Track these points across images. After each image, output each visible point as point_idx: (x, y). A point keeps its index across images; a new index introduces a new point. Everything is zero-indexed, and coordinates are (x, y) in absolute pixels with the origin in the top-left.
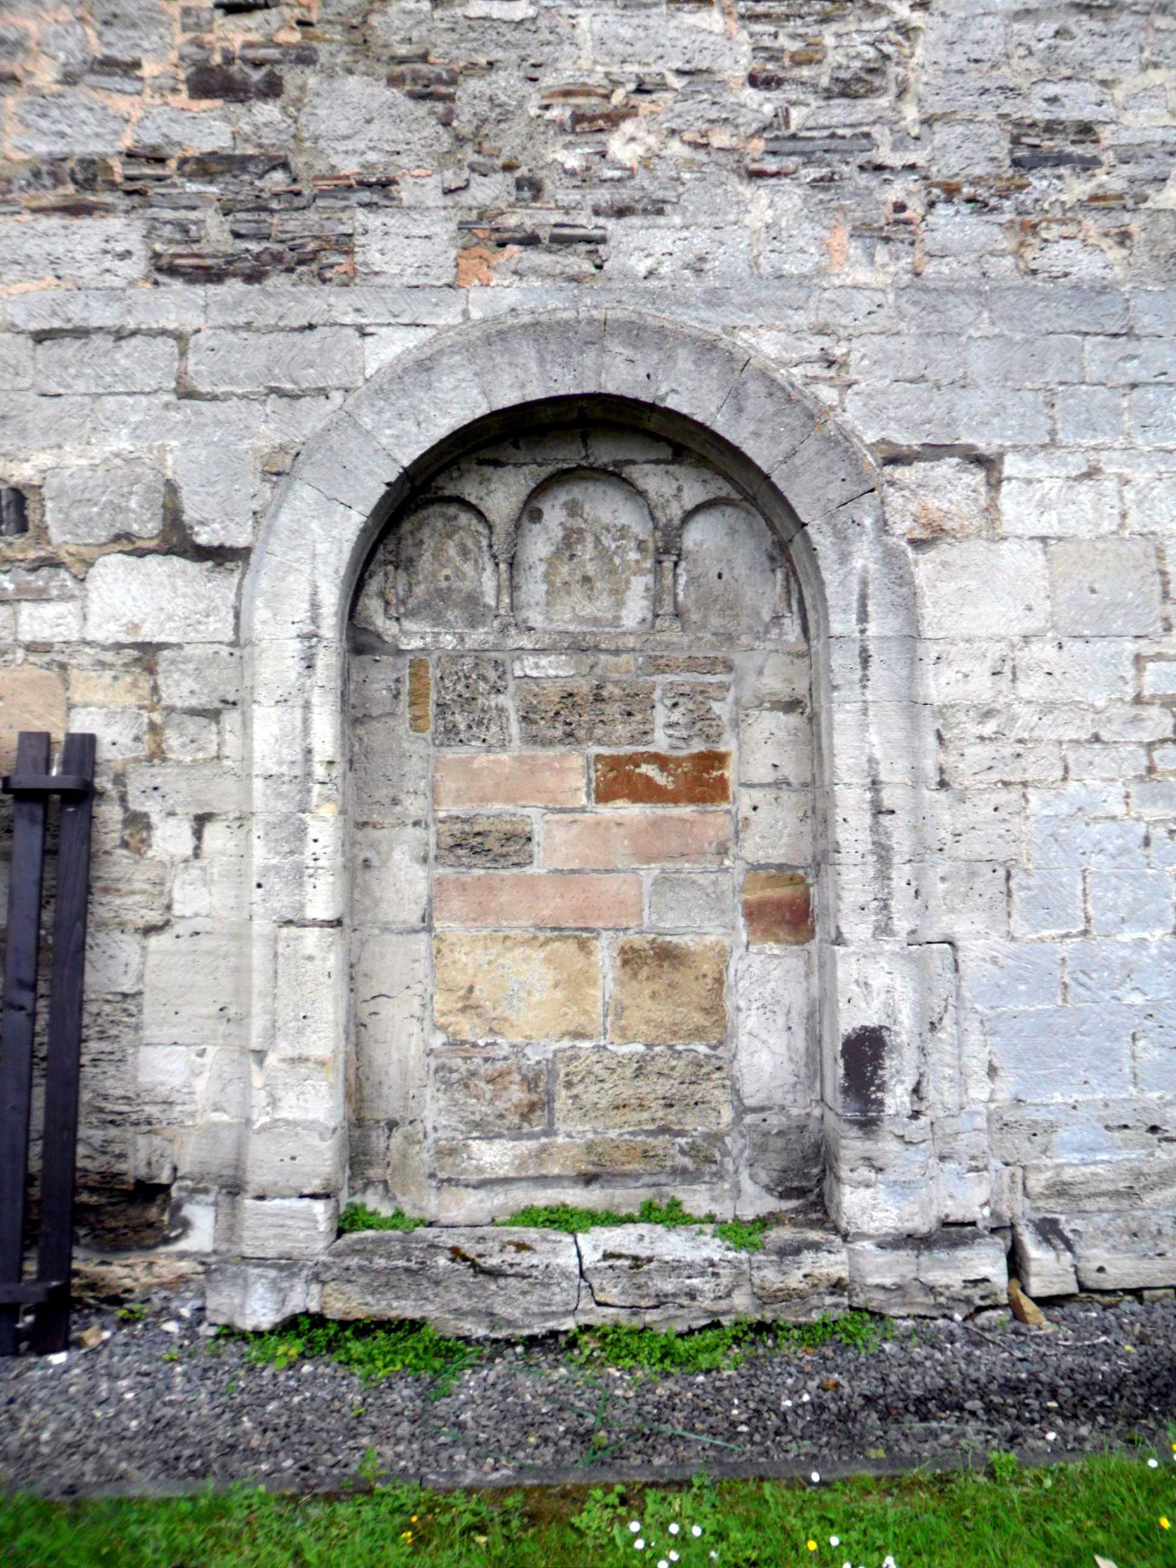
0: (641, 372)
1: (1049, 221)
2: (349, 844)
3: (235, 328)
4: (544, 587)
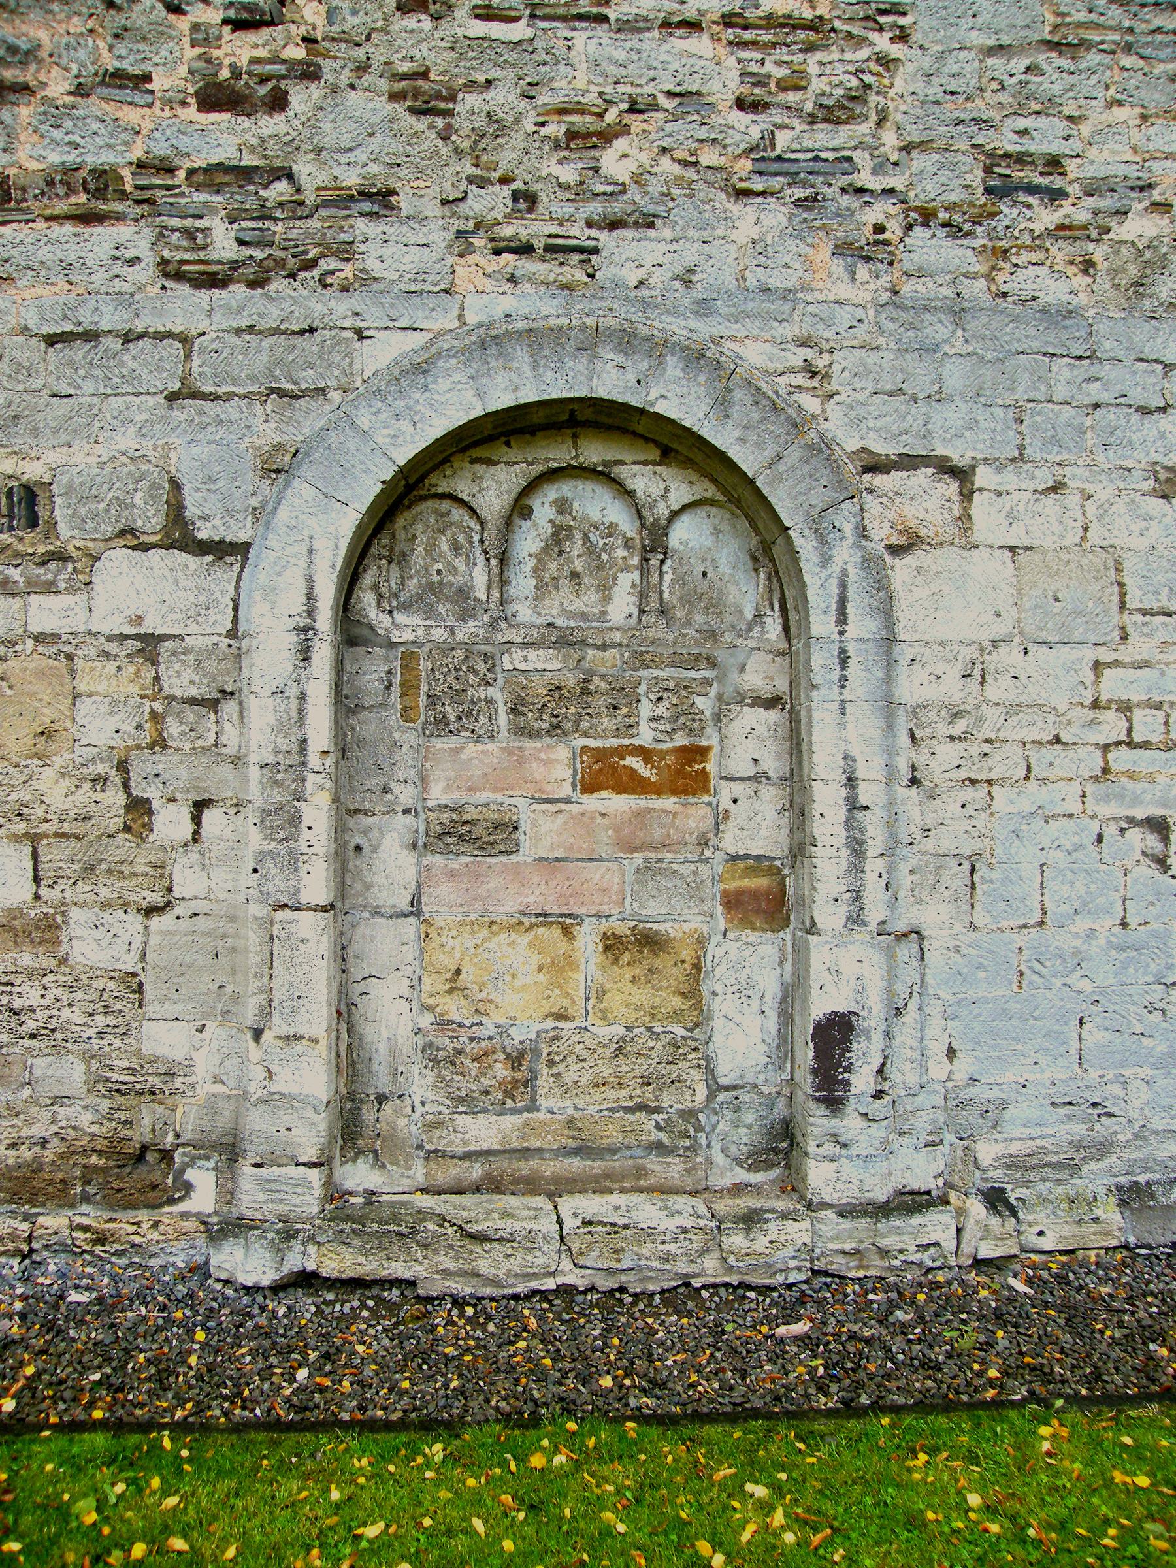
0: (631, 377)
1: (1019, 247)
2: (340, 830)
4: (534, 582)
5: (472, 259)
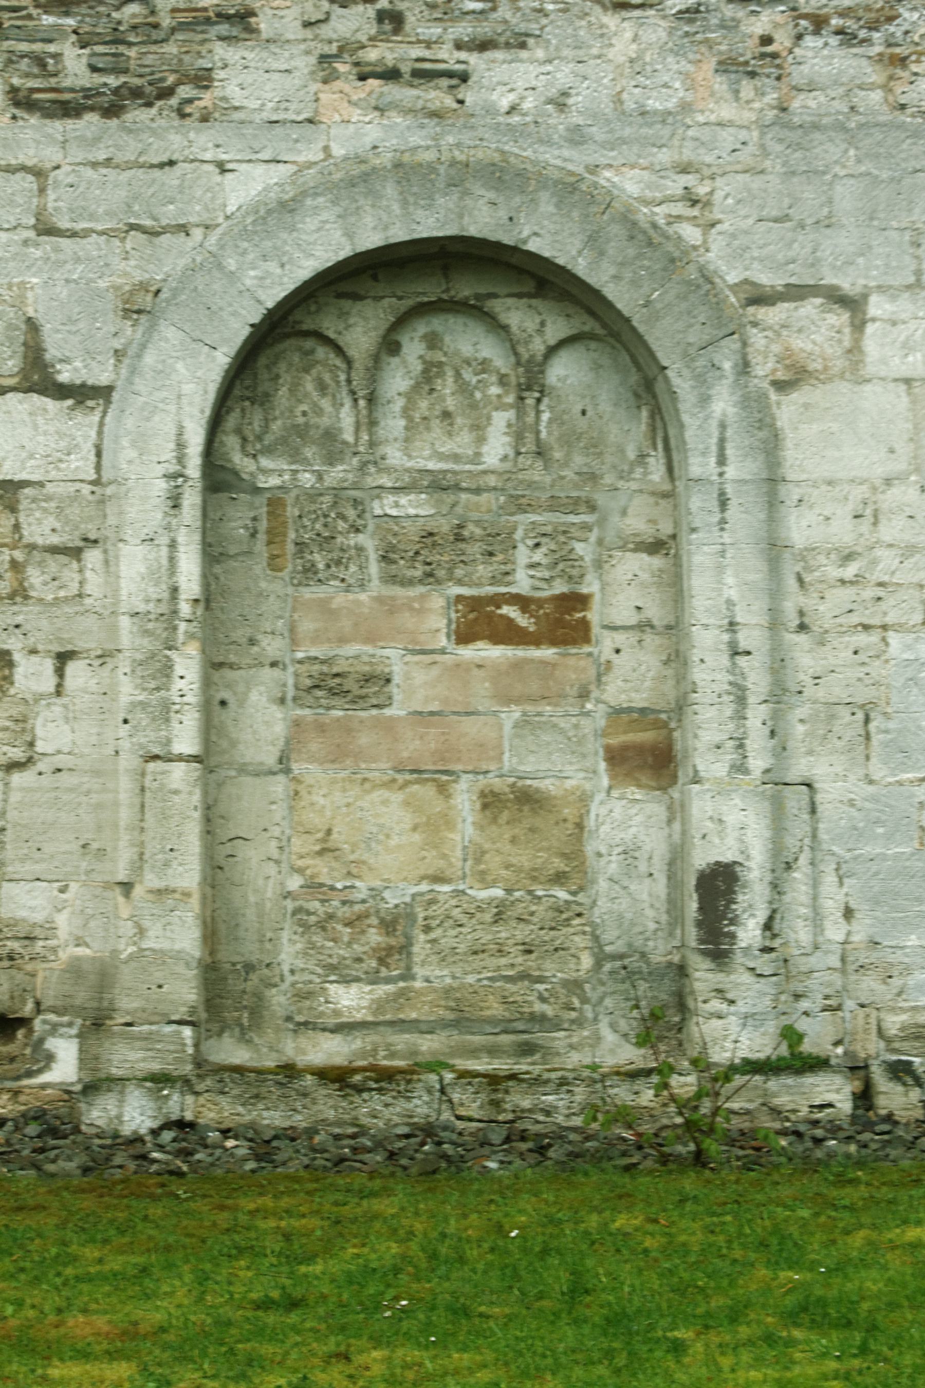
0: (503, 214)
2: (207, 683)
3: (94, 165)
4: (403, 423)
5: (338, 85)
